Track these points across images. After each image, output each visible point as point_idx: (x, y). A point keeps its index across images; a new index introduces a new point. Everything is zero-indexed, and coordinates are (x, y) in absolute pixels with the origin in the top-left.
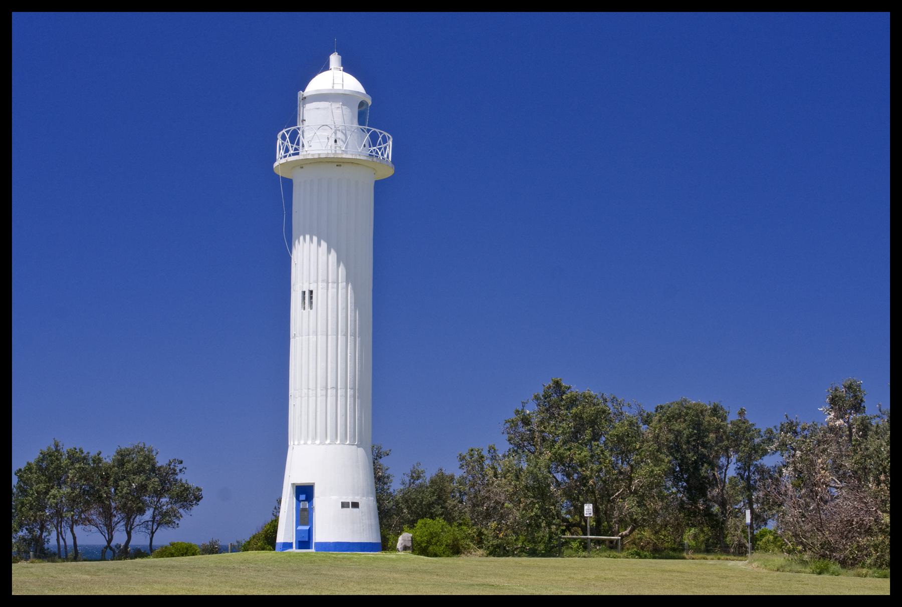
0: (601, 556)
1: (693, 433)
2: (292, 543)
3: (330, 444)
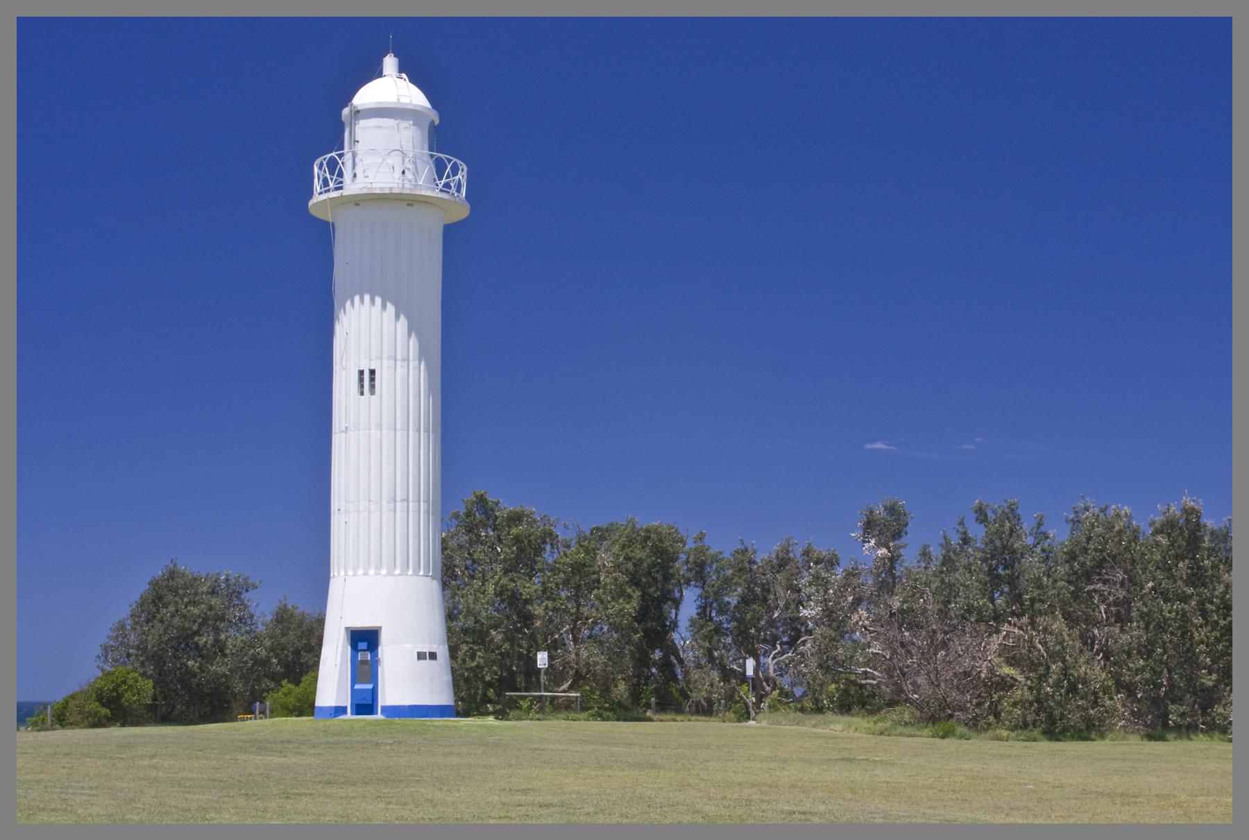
0: (557, 718)
1: (656, 563)
2: (346, 707)
3: (400, 575)
